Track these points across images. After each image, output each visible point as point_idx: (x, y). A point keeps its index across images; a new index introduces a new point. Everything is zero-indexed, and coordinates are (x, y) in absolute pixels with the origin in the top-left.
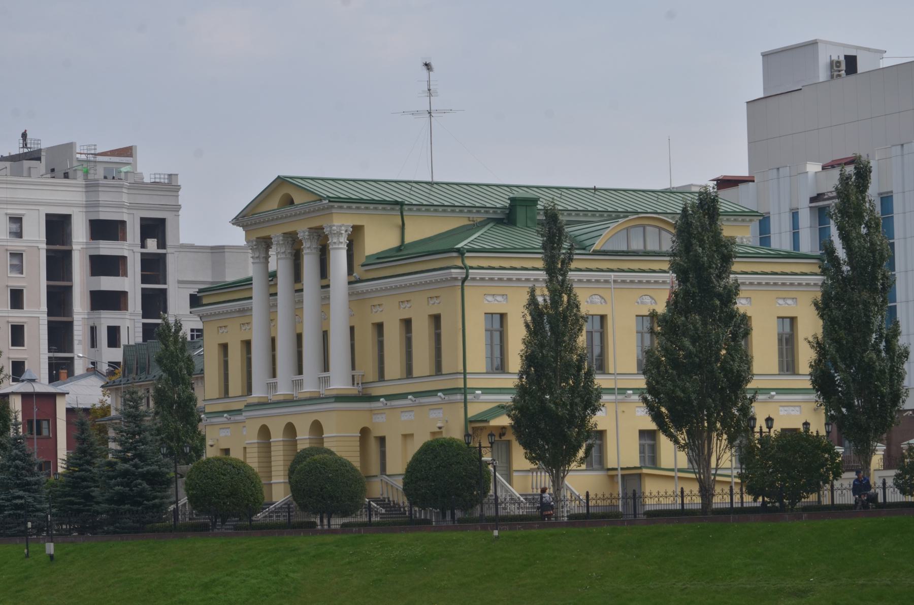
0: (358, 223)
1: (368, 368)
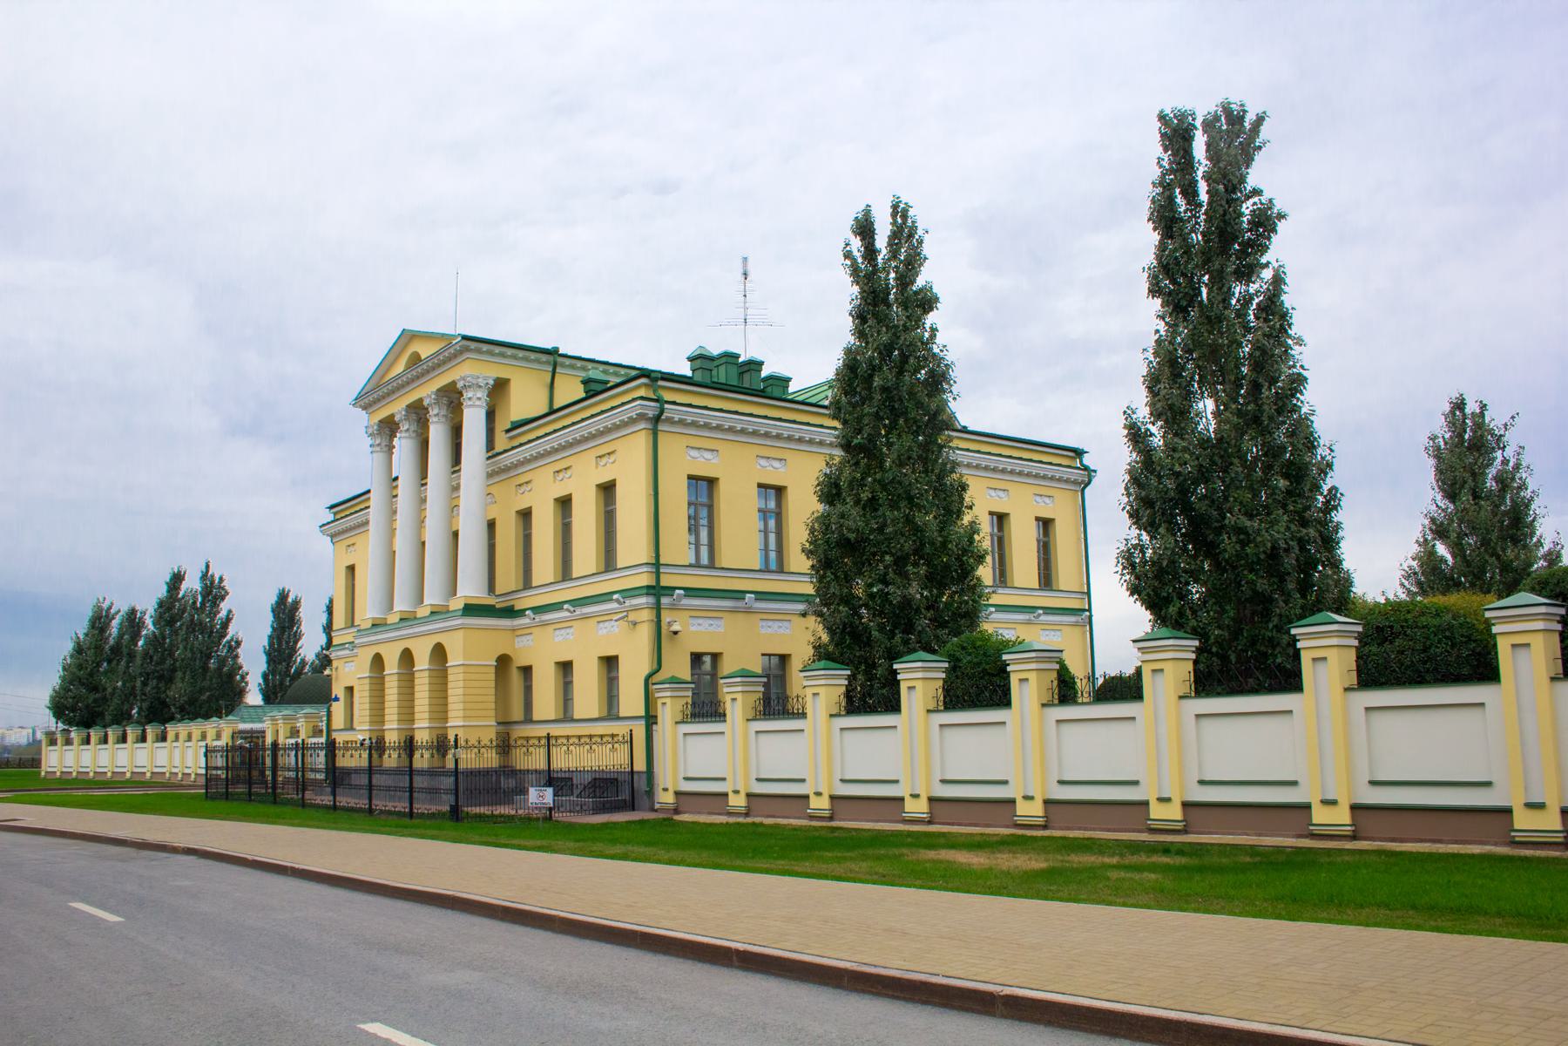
0: (503, 373)
1: (508, 578)
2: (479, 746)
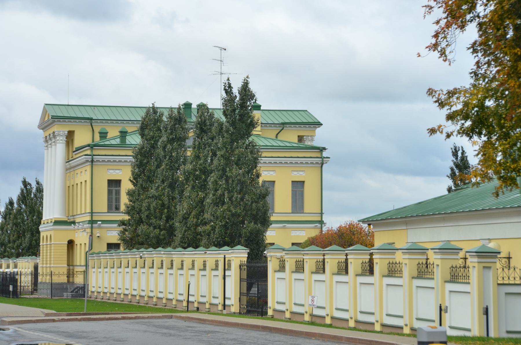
2: (59, 275)
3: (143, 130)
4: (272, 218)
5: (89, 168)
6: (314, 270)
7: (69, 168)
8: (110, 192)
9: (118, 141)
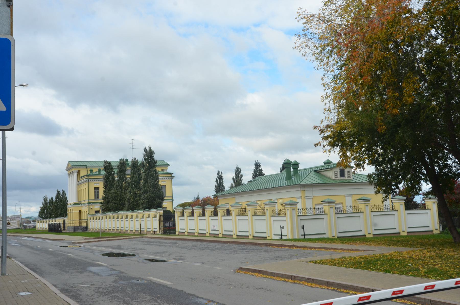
3: (105, 169)
4: (165, 198)
5: (87, 183)
6: (210, 215)
7: (79, 184)
8: (95, 192)
9: (97, 173)
